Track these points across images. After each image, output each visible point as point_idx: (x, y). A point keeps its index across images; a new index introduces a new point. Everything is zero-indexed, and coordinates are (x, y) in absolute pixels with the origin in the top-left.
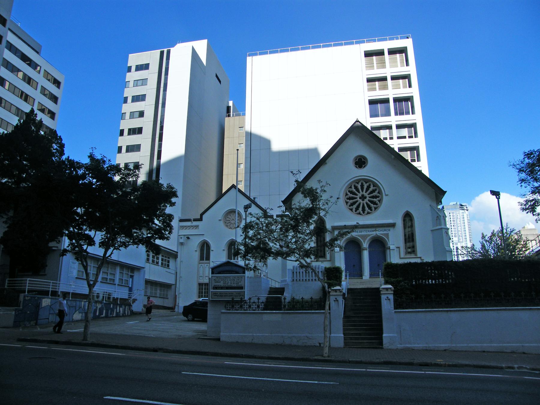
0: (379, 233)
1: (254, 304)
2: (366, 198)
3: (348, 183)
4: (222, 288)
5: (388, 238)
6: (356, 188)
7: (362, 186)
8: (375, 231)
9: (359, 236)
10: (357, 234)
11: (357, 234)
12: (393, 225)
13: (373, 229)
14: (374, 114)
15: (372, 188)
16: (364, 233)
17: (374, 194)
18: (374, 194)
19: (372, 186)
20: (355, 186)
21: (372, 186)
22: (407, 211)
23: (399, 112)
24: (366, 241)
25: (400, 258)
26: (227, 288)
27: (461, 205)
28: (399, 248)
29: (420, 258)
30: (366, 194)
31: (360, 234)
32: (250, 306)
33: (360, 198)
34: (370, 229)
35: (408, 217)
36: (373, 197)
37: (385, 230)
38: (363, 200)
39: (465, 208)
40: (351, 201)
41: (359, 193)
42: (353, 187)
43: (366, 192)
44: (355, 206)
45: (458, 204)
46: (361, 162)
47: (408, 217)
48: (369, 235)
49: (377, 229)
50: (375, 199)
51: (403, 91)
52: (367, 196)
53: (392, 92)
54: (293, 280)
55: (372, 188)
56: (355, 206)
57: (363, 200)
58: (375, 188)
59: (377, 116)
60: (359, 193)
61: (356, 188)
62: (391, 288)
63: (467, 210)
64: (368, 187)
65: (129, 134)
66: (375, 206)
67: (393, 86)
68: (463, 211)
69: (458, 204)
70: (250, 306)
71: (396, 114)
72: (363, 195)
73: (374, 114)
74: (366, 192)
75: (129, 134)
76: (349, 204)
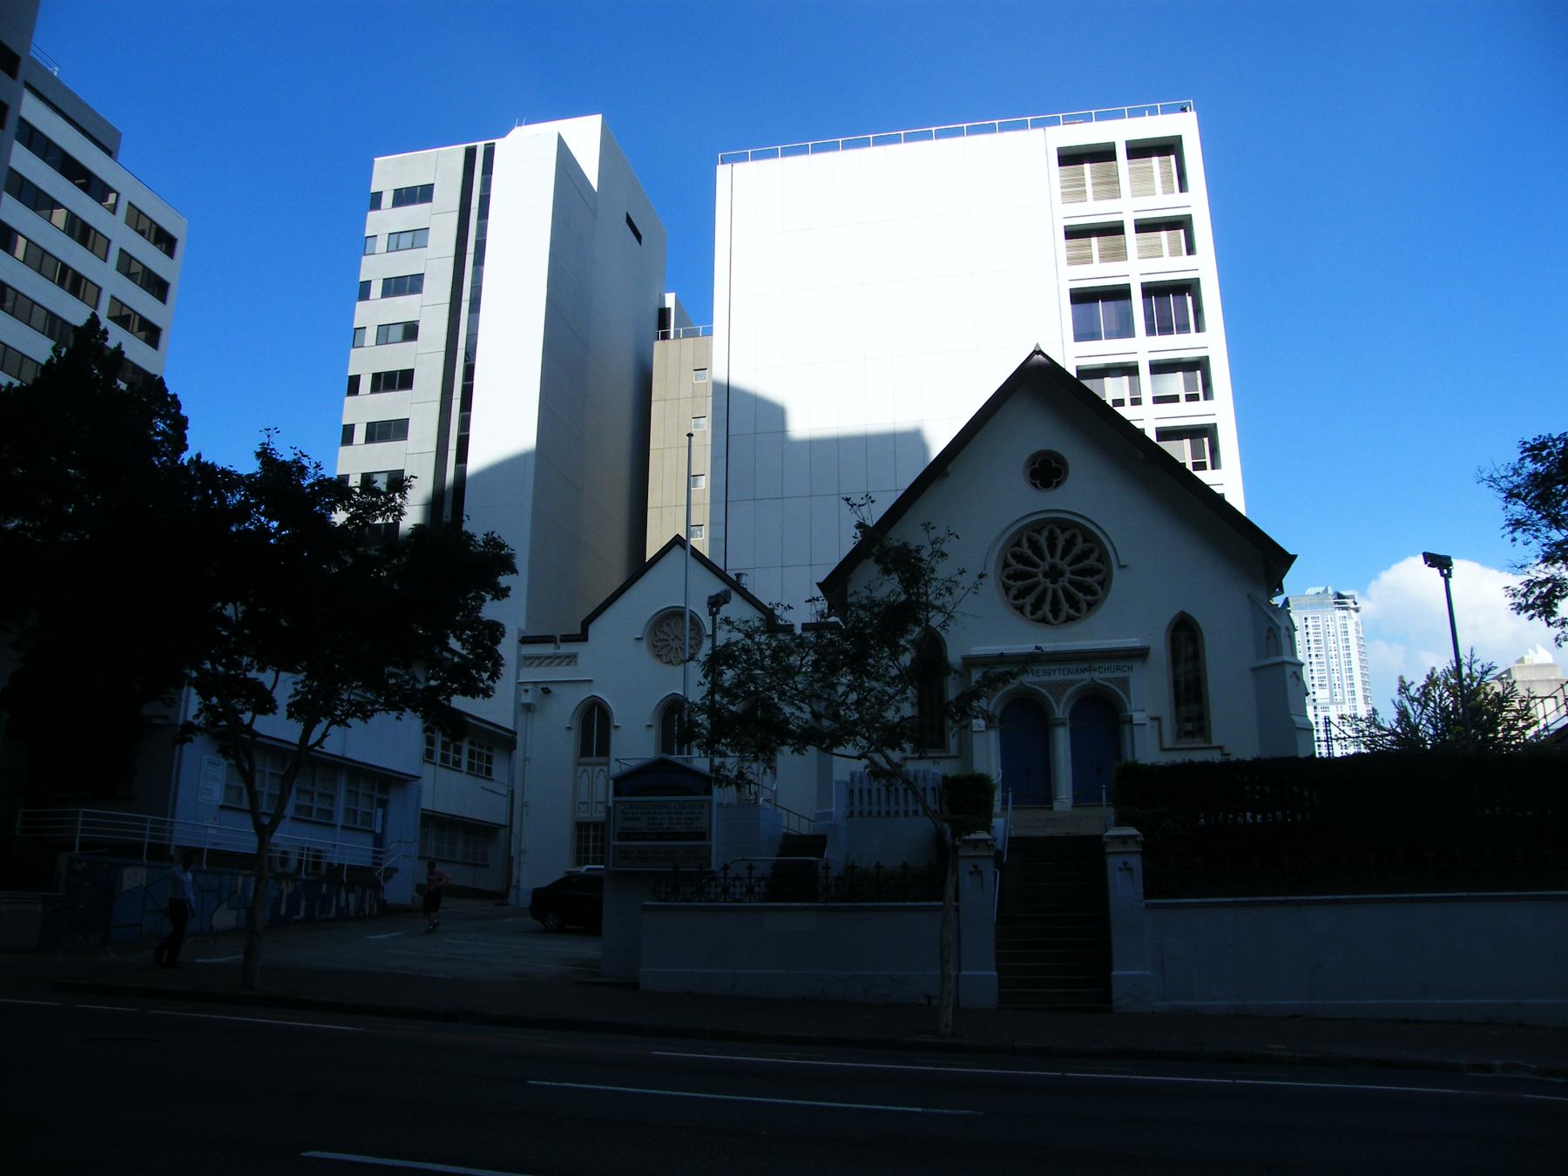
0: (1101, 675)
1: (738, 883)
2: (1062, 574)
3: (1016, 527)
4: (644, 836)
5: (1127, 692)
8: (1090, 669)
9: (1042, 684)
10: (1036, 679)
11: (1036, 679)
13: (1084, 666)
14: (1085, 332)
15: (1080, 546)
16: (1056, 677)
17: (1086, 563)
18: (1086, 563)
19: (1080, 540)
23: (1160, 325)
24: (1063, 701)
25: (1163, 750)
26: (659, 837)
27: (1340, 596)
28: (1157, 719)
29: (1221, 748)
30: (1062, 564)
31: (1115, 675)
32: (725, 890)
33: (1046, 575)
34: (1073, 666)
35: (1184, 632)
37: (1118, 669)
38: (1054, 581)
39: (1350, 603)
40: (1020, 583)
41: (1043, 559)
42: (1025, 543)
44: (1030, 599)
45: (1330, 591)
46: (1047, 471)
47: (1184, 632)
48: (1071, 683)
49: (1096, 665)
50: (1088, 579)
51: (1169, 265)
52: (1068, 575)
53: (1138, 266)
54: (852, 813)
55: (1080, 546)
56: (1030, 599)
57: (1054, 581)
58: (1088, 545)
59: (1094, 336)
60: (1043, 559)
61: (1034, 546)
62: (1134, 837)
63: (1357, 610)
64: (1070, 544)
65: (375, 388)
66: (1089, 597)
67: (1140, 249)
68: (1345, 613)
69: (1330, 591)
70: (725, 890)
71: (1150, 331)
72: (1053, 567)
73: (1085, 332)
75: (375, 388)
76: (1013, 592)
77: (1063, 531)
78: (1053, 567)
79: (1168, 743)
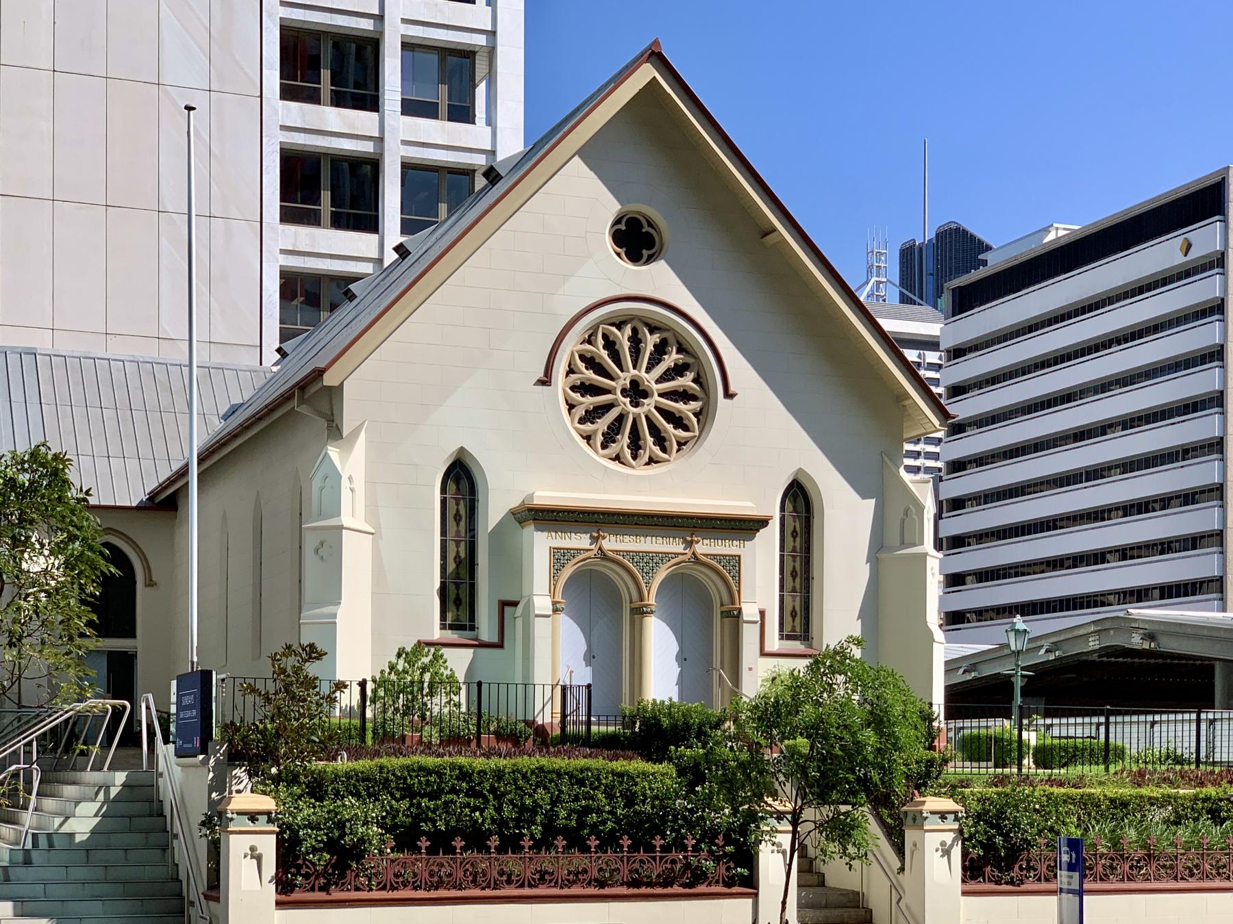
2: (646, 394)
6: (610, 345)
7: (636, 340)
12: (746, 527)
20: (605, 337)
21: (695, 405)
22: (462, 450)
25: (763, 654)
33: (624, 392)
35: (799, 498)
36: (636, 352)
43: (648, 370)
44: (602, 424)
47: (799, 498)
48: (666, 556)
50: (680, 406)
61: (610, 345)
62: (955, 813)
64: (683, 396)
72: (635, 383)
74: (648, 370)
76: (580, 412)
77: (651, 332)
78: (635, 383)
79: (774, 643)
